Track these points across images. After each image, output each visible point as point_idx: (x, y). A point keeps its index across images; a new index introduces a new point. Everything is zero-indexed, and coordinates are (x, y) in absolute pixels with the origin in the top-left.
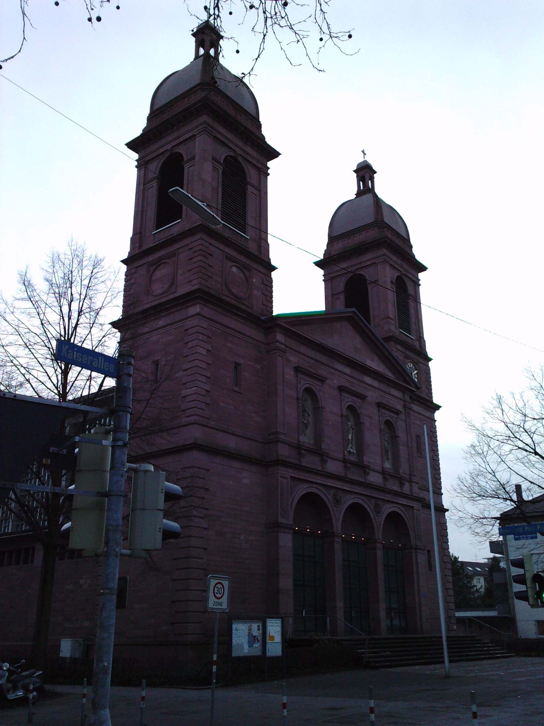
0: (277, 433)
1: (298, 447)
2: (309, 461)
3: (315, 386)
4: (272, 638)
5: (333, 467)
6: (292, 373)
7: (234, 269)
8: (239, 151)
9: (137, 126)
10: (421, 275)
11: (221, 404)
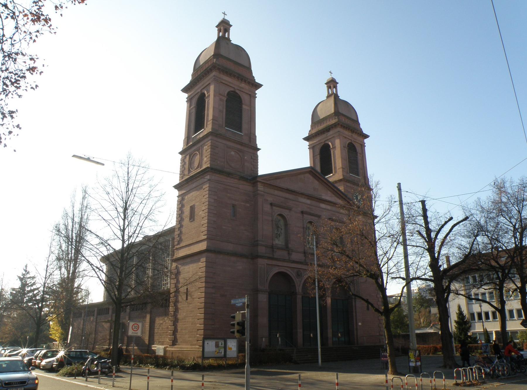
0: (257, 241)
1: (272, 248)
2: (279, 254)
3: (285, 213)
4: (231, 349)
5: (295, 256)
6: (269, 206)
7: (233, 153)
8: (236, 87)
9: (187, 79)
10: (366, 141)
11: (224, 227)
